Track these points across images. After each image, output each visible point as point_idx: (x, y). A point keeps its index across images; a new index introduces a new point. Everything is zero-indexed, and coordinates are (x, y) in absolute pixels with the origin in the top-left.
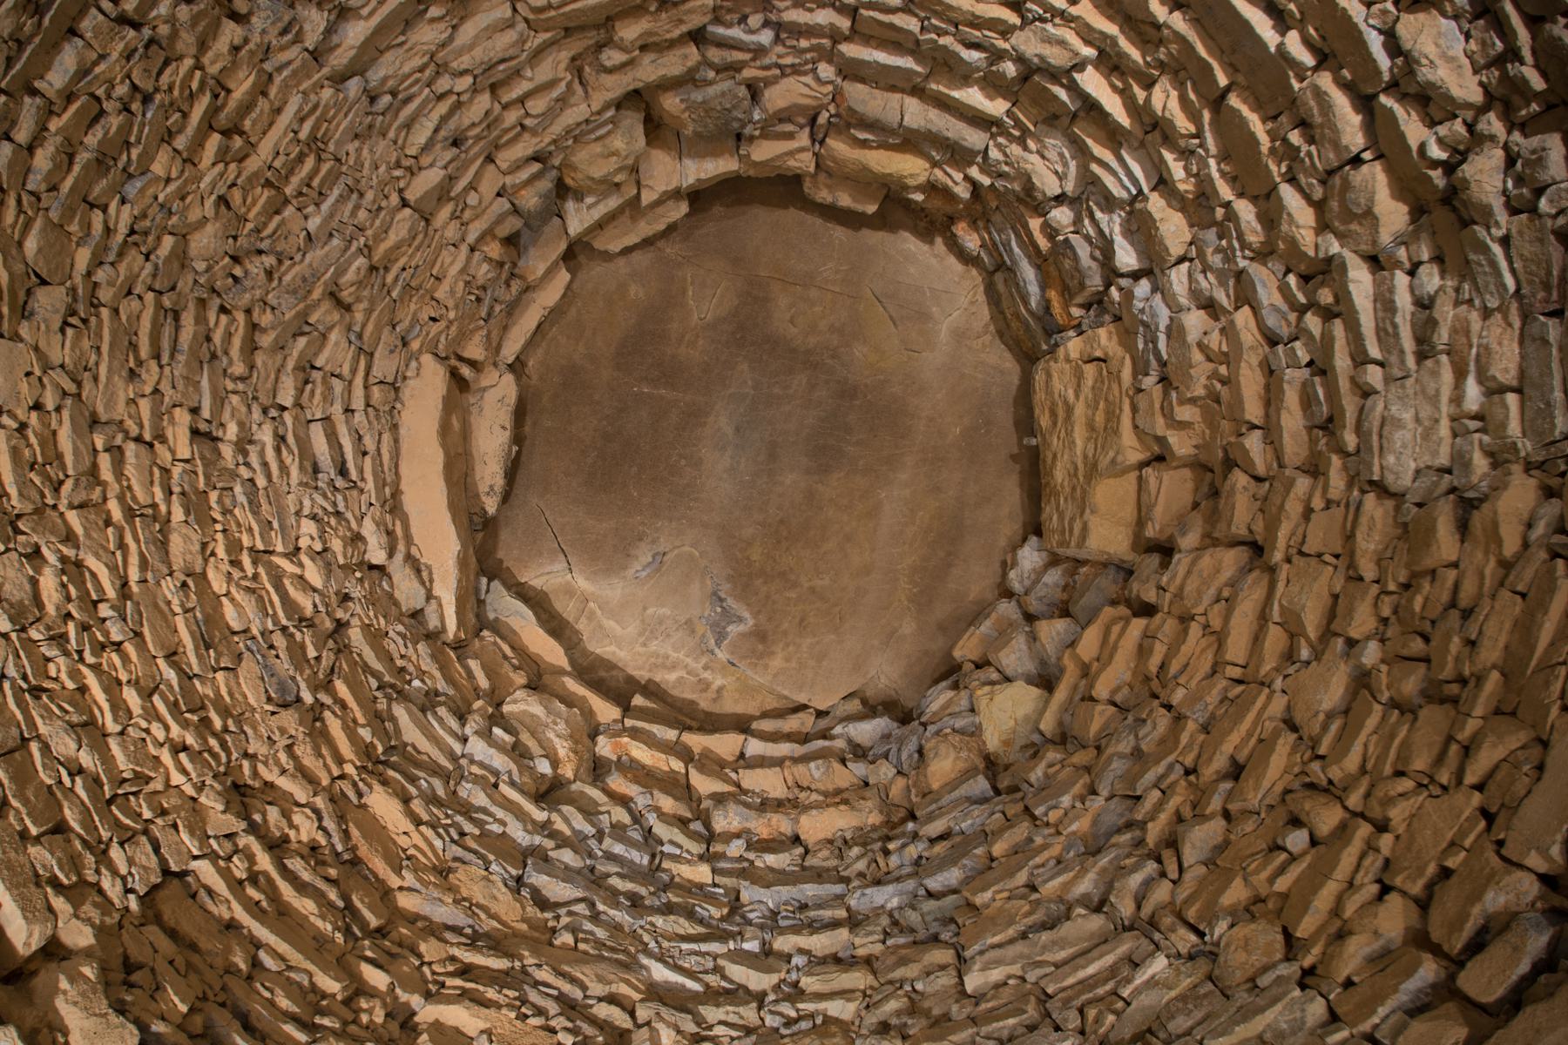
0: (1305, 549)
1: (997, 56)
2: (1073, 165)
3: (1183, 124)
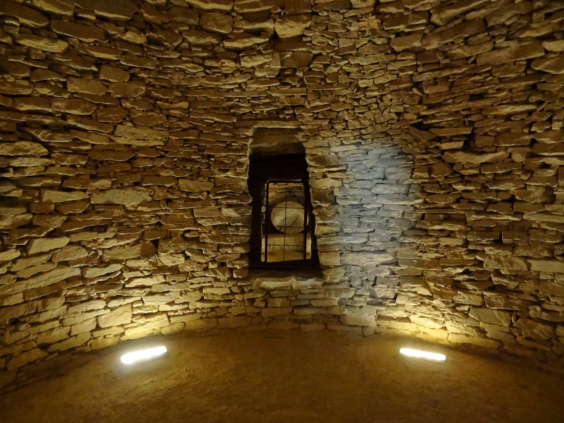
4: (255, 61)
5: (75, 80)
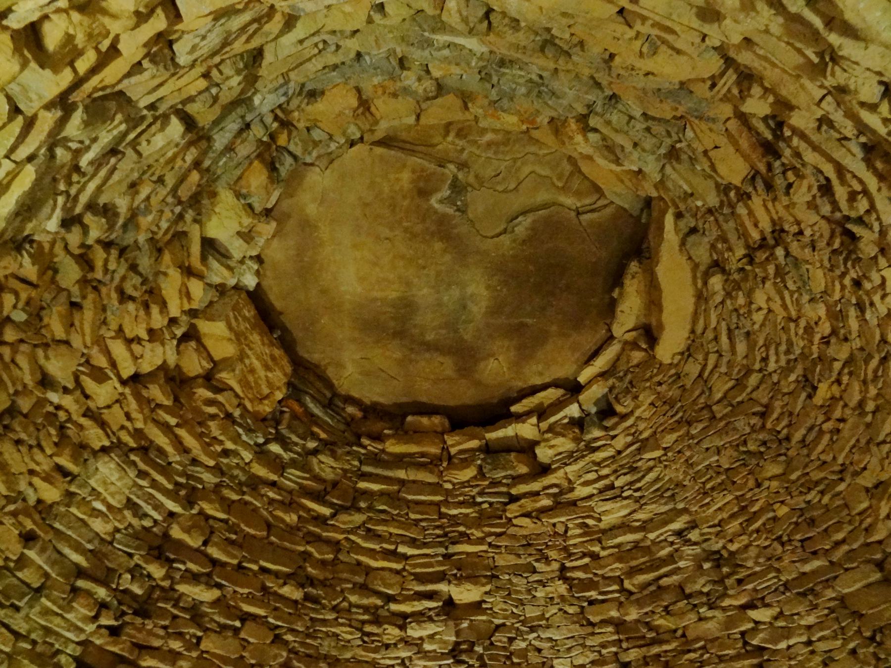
0: (118, 405)
1: (370, 508)
2: (317, 470)
3: (279, 513)
4: (425, 629)
5: (213, 635)
